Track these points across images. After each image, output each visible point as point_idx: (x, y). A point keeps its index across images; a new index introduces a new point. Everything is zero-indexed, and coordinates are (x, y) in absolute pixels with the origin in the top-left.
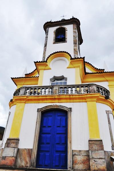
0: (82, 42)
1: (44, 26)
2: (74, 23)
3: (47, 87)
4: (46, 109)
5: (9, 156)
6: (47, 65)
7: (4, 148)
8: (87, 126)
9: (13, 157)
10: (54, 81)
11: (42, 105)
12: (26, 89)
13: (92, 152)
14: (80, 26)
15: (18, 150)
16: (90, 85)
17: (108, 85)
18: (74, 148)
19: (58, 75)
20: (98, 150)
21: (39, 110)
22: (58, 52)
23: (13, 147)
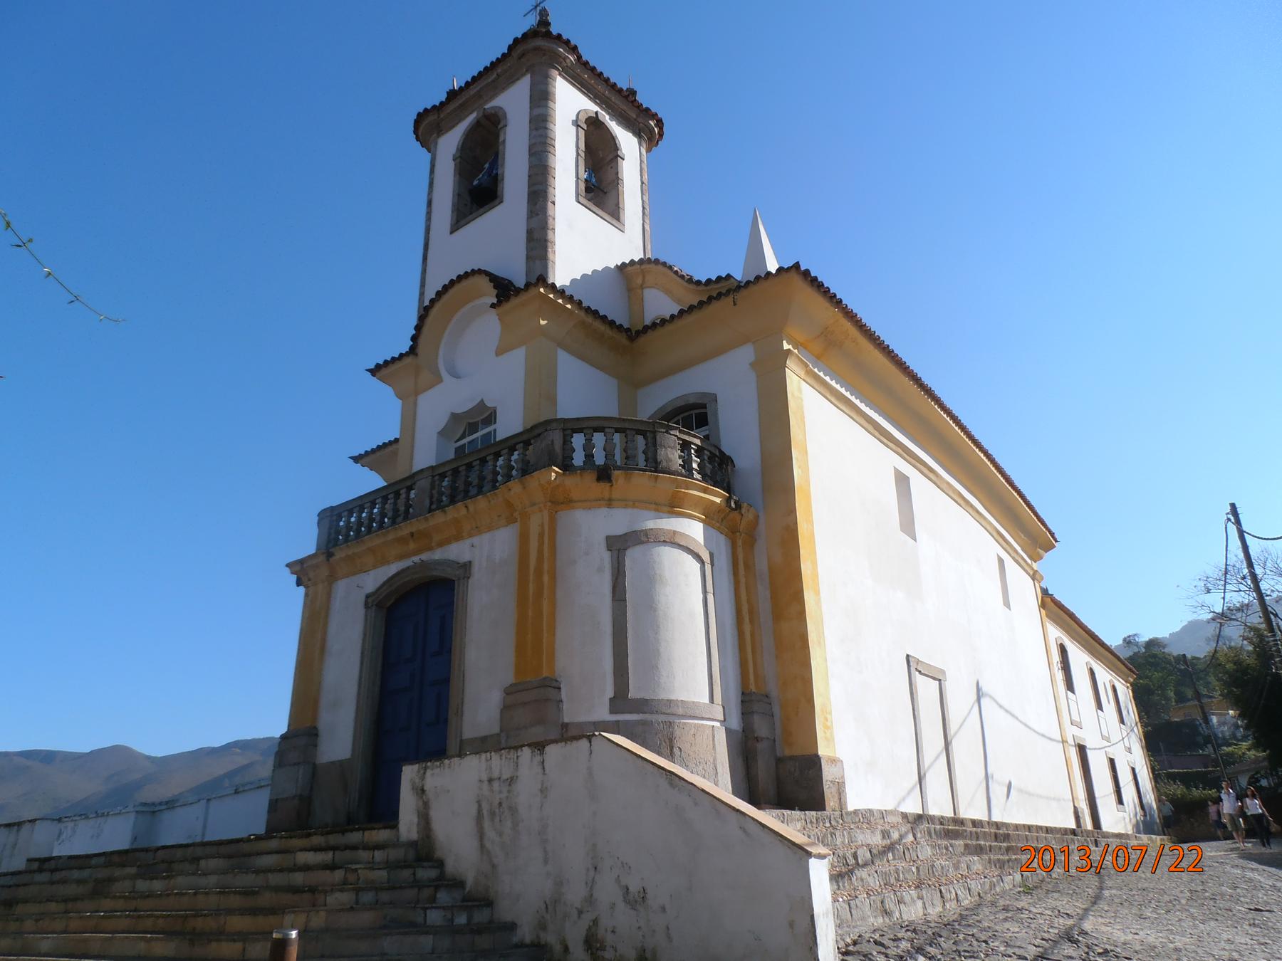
1: (416, 132)
3: (409, 483)
10: (463, 437)
12: (564, 430)
16: (536, 432)
21: (370, 600)
22: (452, 283)
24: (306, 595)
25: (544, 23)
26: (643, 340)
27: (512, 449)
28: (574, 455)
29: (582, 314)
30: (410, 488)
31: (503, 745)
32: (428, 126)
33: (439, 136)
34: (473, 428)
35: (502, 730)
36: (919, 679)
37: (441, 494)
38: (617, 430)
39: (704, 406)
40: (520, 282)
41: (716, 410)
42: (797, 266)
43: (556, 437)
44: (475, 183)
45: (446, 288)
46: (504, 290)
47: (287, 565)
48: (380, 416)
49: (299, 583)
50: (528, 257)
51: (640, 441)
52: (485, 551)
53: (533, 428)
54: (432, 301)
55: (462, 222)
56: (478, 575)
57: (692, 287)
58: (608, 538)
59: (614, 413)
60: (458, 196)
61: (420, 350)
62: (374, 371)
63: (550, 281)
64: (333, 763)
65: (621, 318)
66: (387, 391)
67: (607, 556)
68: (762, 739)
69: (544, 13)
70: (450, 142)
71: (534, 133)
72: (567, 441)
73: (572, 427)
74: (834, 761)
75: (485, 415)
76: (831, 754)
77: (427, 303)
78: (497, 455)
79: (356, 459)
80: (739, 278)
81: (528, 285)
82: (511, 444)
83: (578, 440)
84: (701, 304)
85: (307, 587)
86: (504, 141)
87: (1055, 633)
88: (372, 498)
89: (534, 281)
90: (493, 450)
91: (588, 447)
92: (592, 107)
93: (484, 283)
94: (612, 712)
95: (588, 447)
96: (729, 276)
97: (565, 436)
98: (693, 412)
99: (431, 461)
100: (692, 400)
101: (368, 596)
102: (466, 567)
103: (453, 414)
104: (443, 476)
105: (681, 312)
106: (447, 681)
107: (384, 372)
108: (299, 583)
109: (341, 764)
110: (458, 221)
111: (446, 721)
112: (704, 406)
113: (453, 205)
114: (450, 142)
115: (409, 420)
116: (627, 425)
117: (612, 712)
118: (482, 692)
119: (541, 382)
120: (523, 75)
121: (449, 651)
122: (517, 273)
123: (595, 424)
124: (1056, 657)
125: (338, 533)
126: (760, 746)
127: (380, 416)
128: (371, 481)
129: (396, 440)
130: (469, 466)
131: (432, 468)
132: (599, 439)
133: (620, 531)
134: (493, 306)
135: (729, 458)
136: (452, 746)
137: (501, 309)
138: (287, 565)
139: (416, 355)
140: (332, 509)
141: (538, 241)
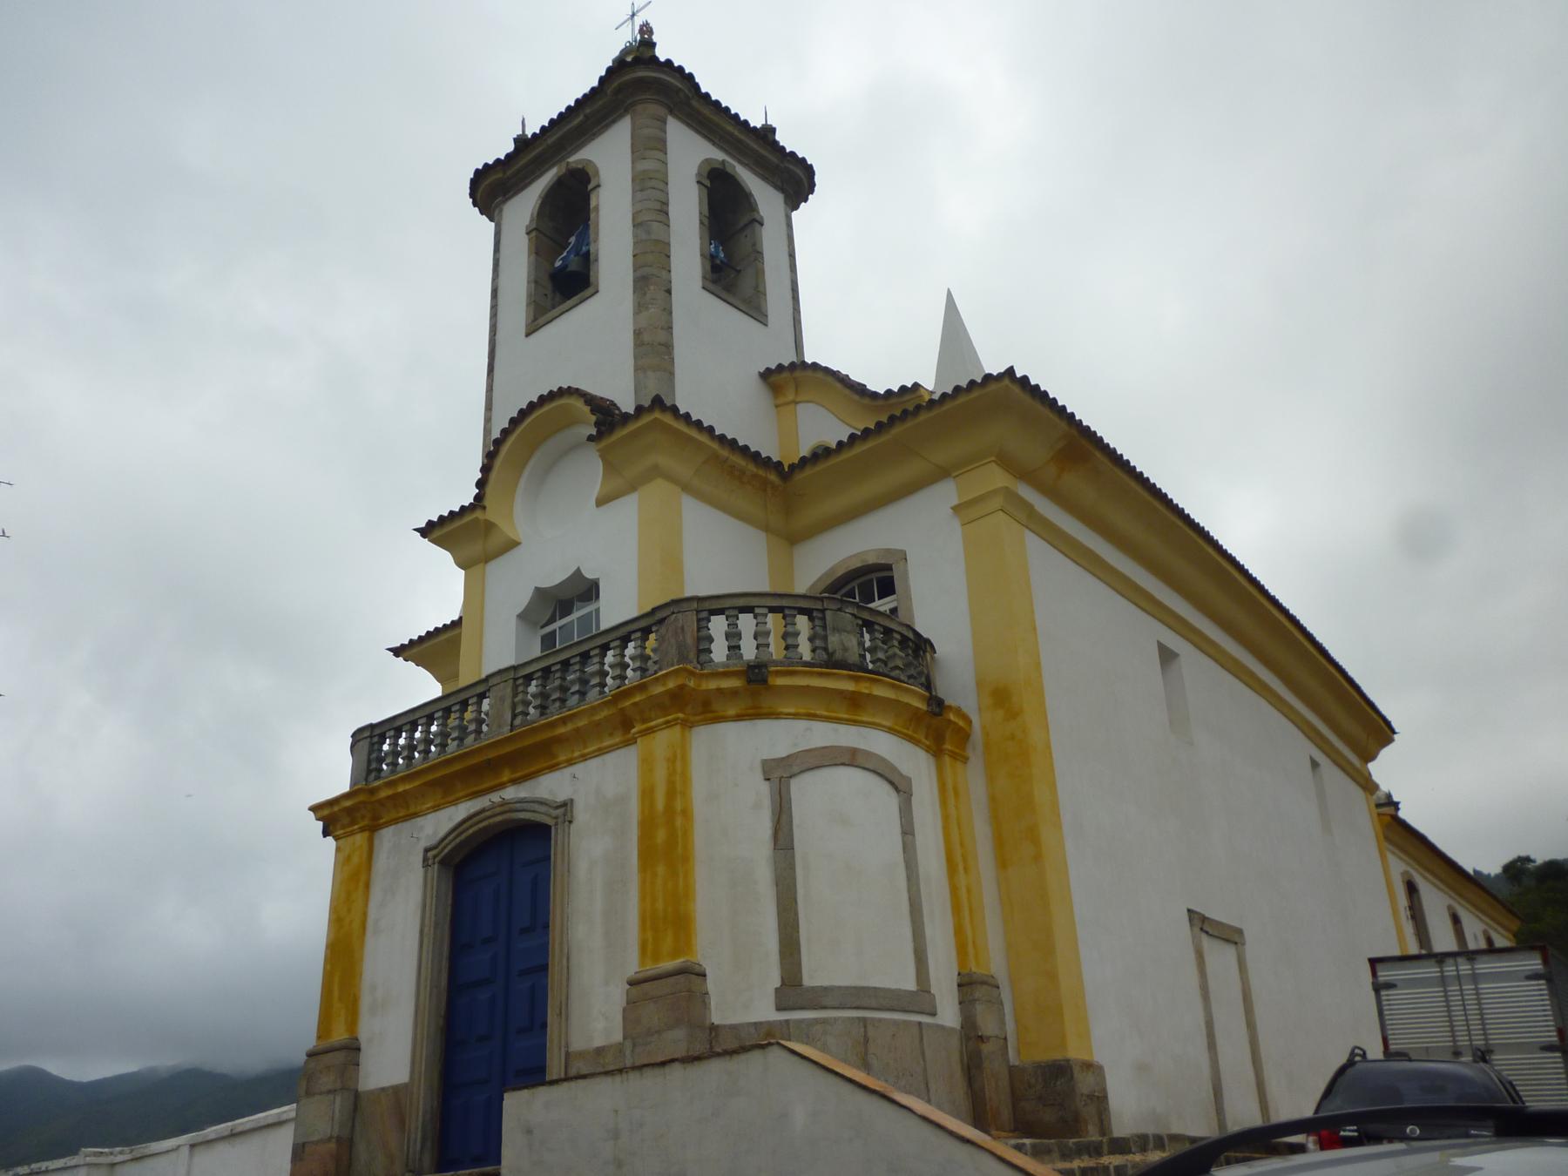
0: (812, 191)
1: (472, 195)
2: (633, 104)
3: (480, 689)
4: (463, 837)
5: (315, 1138)
6: (489, 526)
7: (1401, 835)
8: (799, 857)
9: (330, 1139)
10: (552, 620)
11: (439, 823)
12: (698, 612)
13: (634, 1045)
14: (707, 84)
15: (357, 1095)
16: (659, 616)
17: (955, 502)
18: (577, 1044)
19: (554, 575)
20: (658, 1032)
21: (430, 854)
22: (532, 407)
23: (329, 1092)
24: (338, 849)
25: (645, 43)
26: (799, 477)
27: (625, 640)
28: (713, 646)
29: (715, 446)
30: (482, 696)
31: (628, 1063)
32: (490, 188)
33: (505, 201)
34: (565, 607)
35: (625, 1038)
36: (1206, 942)
37: (527, 704)
38: (773, 610)
39: (889, 568)
40: (627, 406)
41: (906, 572)
42: (1011, 371)
43: (690, 621)
44: (558, 264)
45: (523, 414)
46: (606, 416)
47: (311, 809)
48: (436, 590)
49: (326, 833)
50: (637, 369)
51: (802, 622)
52: (595, 796)
53: (654, 610)
54: (505, 433)
55: (541, 320)
56: (581, 815)
57: (866, 401)
58: (765, 763)
59: (765, 587)
60: (535, 282)
61: (487, 502)
62: (425, 532)
63: (668, 404)
64: (383, 1089)
65: (767, 446)
66: (444, 557)
67: (765, 788)
68: (988, 1038)
69: (646, 29)
70: (524, 207)
71: (639, 195)
72: (702, 624)
73: (709, 606)
74: (1088, 1066)
75: (581, 591)
76: (1086, 1058)
77: (496, 434)
78: (605, 648)
79: (397, 651)
80: (930, 388)
81: (640, 410)
82: (623, 634)
83: (718, 625)
84: (880, 426)
85: (337, 839)
86: (597, 208)
87: (1398, 866)
88: (428, 711)
89: (647, 403)
90: (600, 641)
91: (733, 636)
92: (718, 155)
93: (579, 404)
94: (779, 1008)
95: (733, 636)
96: (916, 386)
97: (699, 620)
98: (874, 576)
99: (509, 660)
100: (872, 560)
101: (427, 850)
102: (567, 805)
103: (537, 589)
104: (528, 678)
105: (852, 437)
106: (544, 968)
107: (437, 533)
108: (326, 833)
109: (396, 1091)
110: (535, 319)
111: (544, 1025)
112: (889, 568)
113: (529, 296)
114: (524, 207)
115: (474, 594)
116: (784, 603)
117: (779, 1008)
118: (594, 991)
119: (663, 551)
120: (621, 117)
121: (546, 926)
122: (623, 394)
123: (741, 602)
124: (1403, 901)
125: (381, 760)
126: (986, 1048)
127: (436, 590)
128: (423, 687)
129: (456, 624)
130: (566, 664)
131: (514, 668)
132: (746, 623)
133: (781, 752)
134: (590, 438)
135: (928, 642)
136: (555, 1068)
137: (604, 443)
138: (311, 809)
139: (484, 508)
140: (372, 727)
141: (654, 348)
